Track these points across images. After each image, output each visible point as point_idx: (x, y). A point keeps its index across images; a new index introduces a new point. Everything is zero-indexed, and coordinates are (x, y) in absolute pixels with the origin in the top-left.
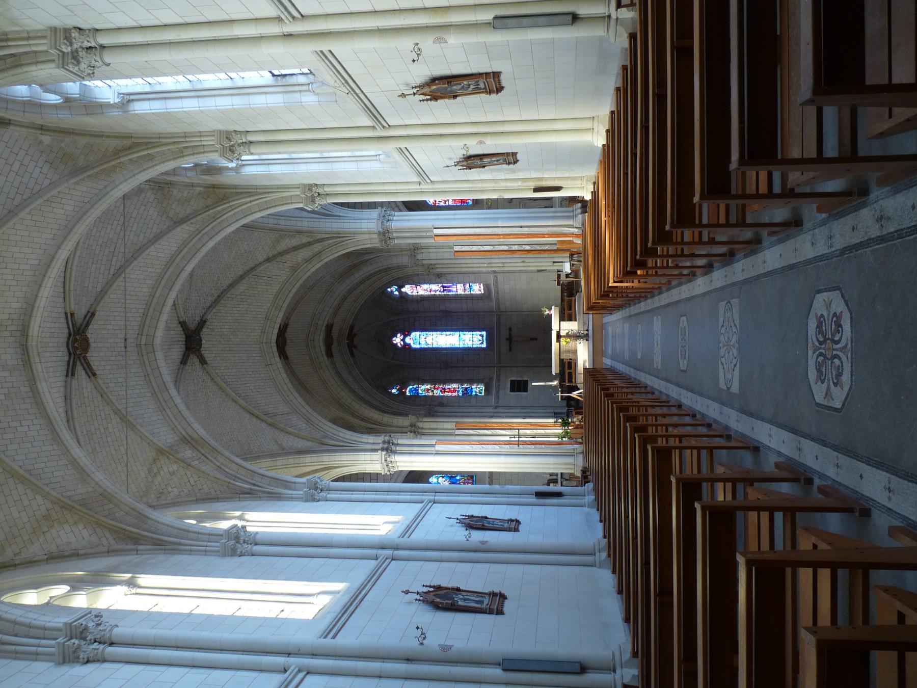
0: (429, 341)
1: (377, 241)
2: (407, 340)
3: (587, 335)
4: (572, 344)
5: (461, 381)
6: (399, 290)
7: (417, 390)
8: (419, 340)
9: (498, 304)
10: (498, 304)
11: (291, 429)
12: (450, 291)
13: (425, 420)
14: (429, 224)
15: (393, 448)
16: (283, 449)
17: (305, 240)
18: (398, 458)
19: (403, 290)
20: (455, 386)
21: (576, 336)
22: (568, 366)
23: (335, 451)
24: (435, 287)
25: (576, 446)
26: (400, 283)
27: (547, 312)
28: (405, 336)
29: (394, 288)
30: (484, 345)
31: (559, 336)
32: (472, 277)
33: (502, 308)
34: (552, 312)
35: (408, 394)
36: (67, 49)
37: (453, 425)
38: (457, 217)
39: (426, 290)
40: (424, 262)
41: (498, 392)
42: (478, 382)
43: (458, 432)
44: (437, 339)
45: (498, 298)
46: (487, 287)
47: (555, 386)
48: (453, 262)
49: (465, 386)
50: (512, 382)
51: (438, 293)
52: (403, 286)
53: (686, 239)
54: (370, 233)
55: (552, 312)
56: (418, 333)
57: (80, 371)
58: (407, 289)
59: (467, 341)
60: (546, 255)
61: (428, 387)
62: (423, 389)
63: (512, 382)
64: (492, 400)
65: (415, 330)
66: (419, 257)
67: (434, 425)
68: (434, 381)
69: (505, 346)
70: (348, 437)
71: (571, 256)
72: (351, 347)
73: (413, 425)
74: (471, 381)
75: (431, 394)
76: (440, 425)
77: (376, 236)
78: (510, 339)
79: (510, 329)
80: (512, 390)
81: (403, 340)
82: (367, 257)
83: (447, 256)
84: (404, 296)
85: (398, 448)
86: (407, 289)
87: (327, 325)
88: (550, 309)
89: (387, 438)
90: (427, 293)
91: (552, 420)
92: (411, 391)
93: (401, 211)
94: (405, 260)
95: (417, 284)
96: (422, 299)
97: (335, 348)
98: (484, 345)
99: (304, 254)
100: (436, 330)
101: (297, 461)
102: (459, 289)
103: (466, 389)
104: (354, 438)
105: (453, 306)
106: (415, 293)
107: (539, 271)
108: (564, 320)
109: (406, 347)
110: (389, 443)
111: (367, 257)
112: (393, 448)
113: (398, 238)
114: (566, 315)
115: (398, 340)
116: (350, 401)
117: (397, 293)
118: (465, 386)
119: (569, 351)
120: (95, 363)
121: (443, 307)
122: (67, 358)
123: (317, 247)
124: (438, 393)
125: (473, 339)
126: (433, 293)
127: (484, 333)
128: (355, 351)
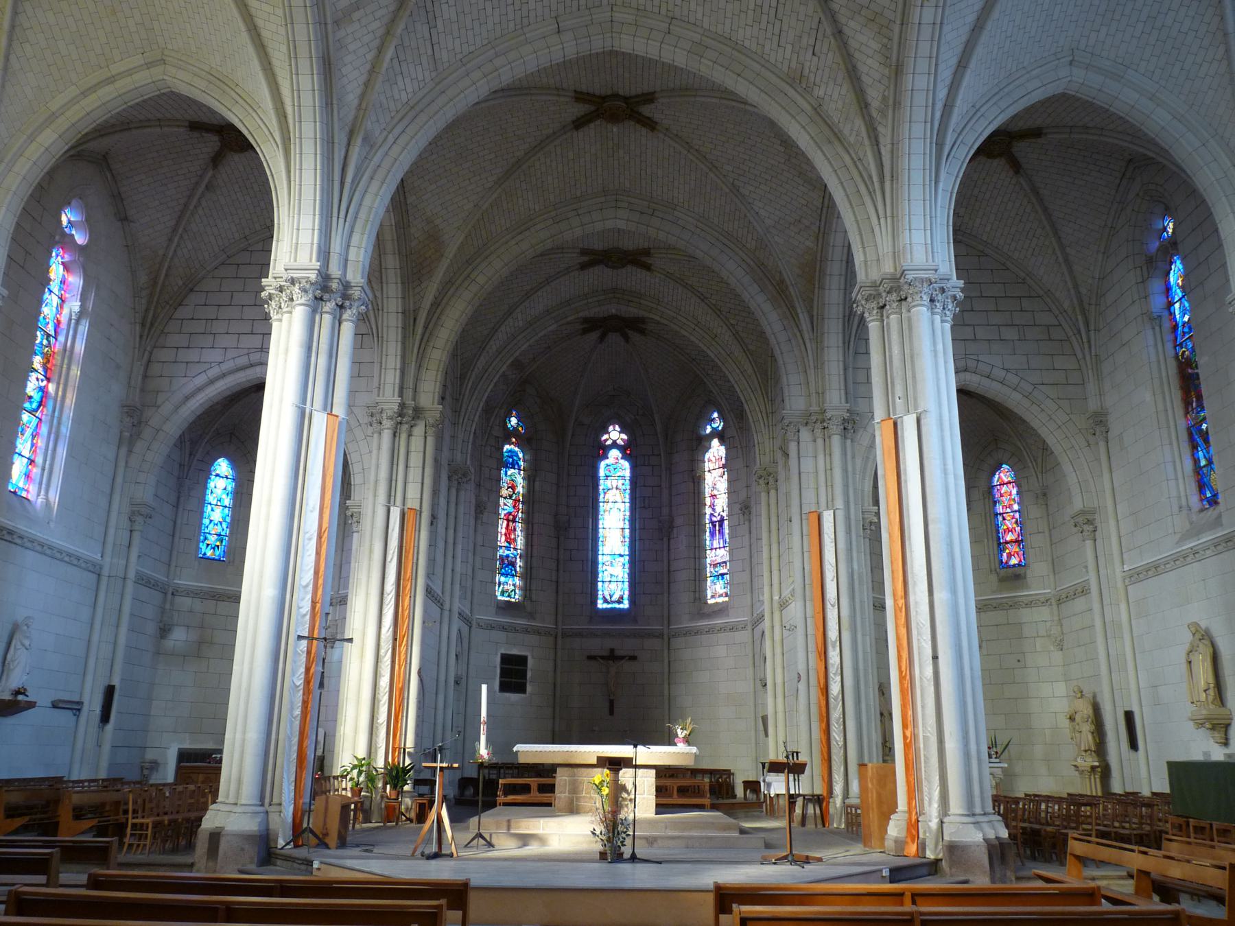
0: (611, 496)
1: (875, 275)
2: (615, 453)
3: (618, 857)
4: (596, 801)
5: (528, 555)
7: (514, 465)
8: (615, 478)
9: (687, 633)
10: (687, 633)
11: (390, 53)
12: (712, 535)
13: (430, 440)
14: (928, 401)
15: (329, 306)
16: (336, 23)
17: (874, 96)
18: (299, 314)
19: (715, 442)
20: (520, 542)
21: (614, 827)
22: (537, 788)
23: (328, 158)
24: (722, 503)
25: (288, 811)
26: (731, 432)
27: (681, 734)
28: (623, 449)
29: (718, 424)
30: (601, 605)
31: (615, 764)
32: (745, 577)
33: (677, 642)
34: (681, 747)
35: (507, 447)
36: (814, 418)
37: (412, 503)
41: (503, 628)
42: (526, 589)
44: (614, 512)
45: (698, 632)
46: (720, 610)
47: (475, 751)
49: (519, 563)
50: (523, 660)
51: (708, 511)
52: (722, 441)
54: (895, 255)
55: (681, 747)
56: (627, 473)
57: (580, 110)
58: (716, 451)
59: (610, 570)
60: (817, 734)
61: (520, 489)
62: (515, 479)
63: (523, 660)
64: (486, 615)
65: (633, 468)
66: (805, 434)
67: (416, 460)
68: (531, 500)
69: (597, 646)
70: (367, 201)
71: (818, 800)
72: (600, 326)
73: (418, 413)
74: (527, 576)
75: (504, 492)
76: (414, 474)
77: (888, 268)
78: (612, 657)
79: (633, 658)
80: (506, 659)
81: (615, 445)
82: (803, 318)
83: (809, 496)
84: (701, 444)
85: (327, 319)
86: (716, 451)
87: (642, 320)
88: (687, 740)
89: (356, 293)
90: (708, 491)
91: (410, 743)
92: (512, 454)
96: (697, 480)
97: (602, 276)
98: (601, 605)
99: (836, 96)
100: (633, 509)
101: (303, 51)
102: (717, 553)
103: (513, 564)
104: (362, 215)
105: (681, 543)
106: (707, 466)
107: (765, 719)
108: (658, 776)
109: (601, 451)
110: (345, 297)
111: (803, 318)
112: (329, 306)
114: (676, 788)
115: (615, 434)
116: (481, 280)
117: (709, 430)
118: (519, 563)
119: (575, 789)
120: (592, 130)
121: (679, 521)
122: (597, 93)
123: (854, 129)
124: (506, 506)
125: (613, 581)
126: (708, 501)
128: (594, 336)
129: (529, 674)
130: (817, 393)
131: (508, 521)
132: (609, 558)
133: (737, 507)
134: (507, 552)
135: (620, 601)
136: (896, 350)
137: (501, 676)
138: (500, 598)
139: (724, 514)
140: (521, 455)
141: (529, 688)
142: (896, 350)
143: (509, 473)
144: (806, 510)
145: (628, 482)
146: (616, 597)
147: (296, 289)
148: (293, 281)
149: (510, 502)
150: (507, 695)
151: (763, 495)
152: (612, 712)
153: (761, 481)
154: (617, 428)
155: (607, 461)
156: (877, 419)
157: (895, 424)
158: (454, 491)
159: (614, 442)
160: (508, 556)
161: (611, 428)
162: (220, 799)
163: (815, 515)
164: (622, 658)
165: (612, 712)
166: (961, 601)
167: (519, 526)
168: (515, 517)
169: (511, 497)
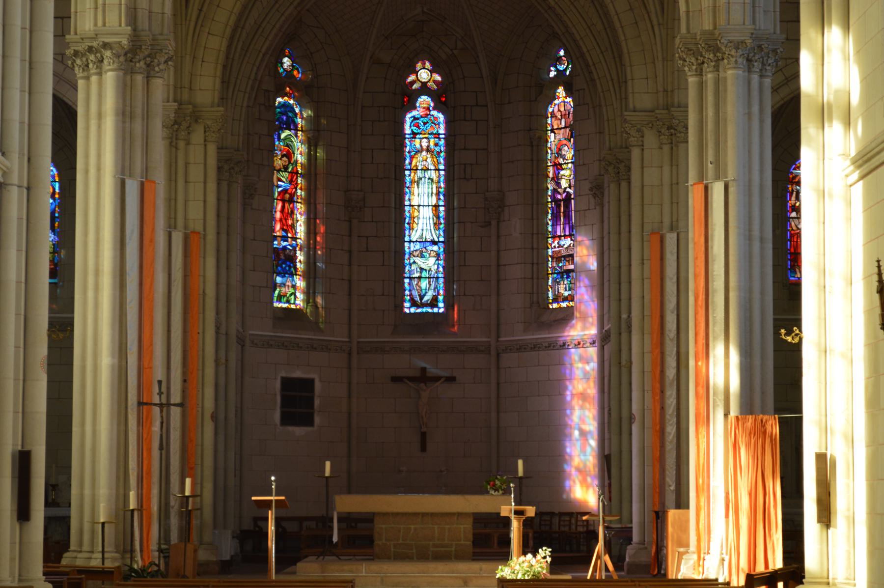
0: (419, 161)
2: (424, 100)
6: (561, 77)
7: (290, 124)
8: (425, 134)
13: (212, 149)
19: (561, 91)
20: (301, 230)
30: (408, 308)
38: (756, 245)
39: (559, 154)
40: (636, 153)
41: (283, 345)
43: (178, 238)
48: (635, 229)
49: (300, 256)
50: (308, 384)
52: (569, 92)
53: (427, 281)
58: (562, 100)
63: (308, 384)
67: (196, 172)
75: (279, 162)
77: (707, 26)
78: (423, 378)
79: (451, 379)
80: (288, 384)
81: (424, 89)
85: (139, 79)
92: (285, 105)
93: (775, 90)
94: (642, 97)
95: (574, 131)
98: (408, 308)
103: (292, 259)
105: (515, 227)
113: (701, 85)
124: (282, 182)
127: (441, 308)
129: (317, 402)
130: (665, 91)
131: (283, 201)
132: (418, 246)
133: (586, 186)
134: (285, 244)
135: (434, 303)
136: (710, 112)
137: (283, 405)
138: (276, 305)
139: (571, 191)
140: (292, 102)
141: (317, 420)
142: (710, 112)
143: (283, 136)
144: (648, 228)
145: (442, 142)
146: (428, 298)
147: (108, 53)
148: (105, 46)
149: (285, 176)
150: (291, 428)
151: (613, 186)
152: (423, 448)
153: (610, 169)
154: (428, 65)
155: (414, 113)
156: (691, 182)
157: (706, 188)
158: (225, 184)
159: (424, 84)
160: (285, 248)
161: (419, 65)
162: (72, 548)
163: (658, 237)
164: (437, 379)
165: (423, 448)
166: (757, 362)
167: (300, 207)
168: (292, 195)
169: (286, 168)
